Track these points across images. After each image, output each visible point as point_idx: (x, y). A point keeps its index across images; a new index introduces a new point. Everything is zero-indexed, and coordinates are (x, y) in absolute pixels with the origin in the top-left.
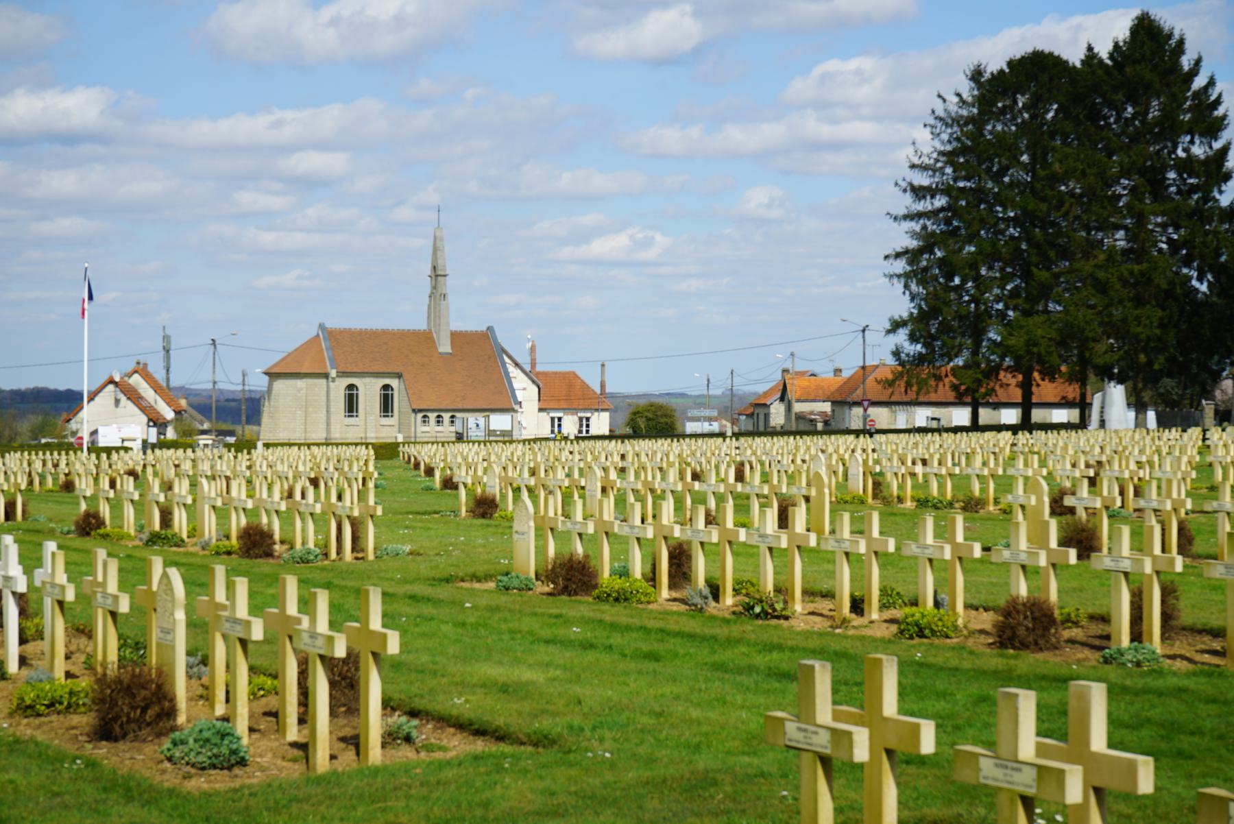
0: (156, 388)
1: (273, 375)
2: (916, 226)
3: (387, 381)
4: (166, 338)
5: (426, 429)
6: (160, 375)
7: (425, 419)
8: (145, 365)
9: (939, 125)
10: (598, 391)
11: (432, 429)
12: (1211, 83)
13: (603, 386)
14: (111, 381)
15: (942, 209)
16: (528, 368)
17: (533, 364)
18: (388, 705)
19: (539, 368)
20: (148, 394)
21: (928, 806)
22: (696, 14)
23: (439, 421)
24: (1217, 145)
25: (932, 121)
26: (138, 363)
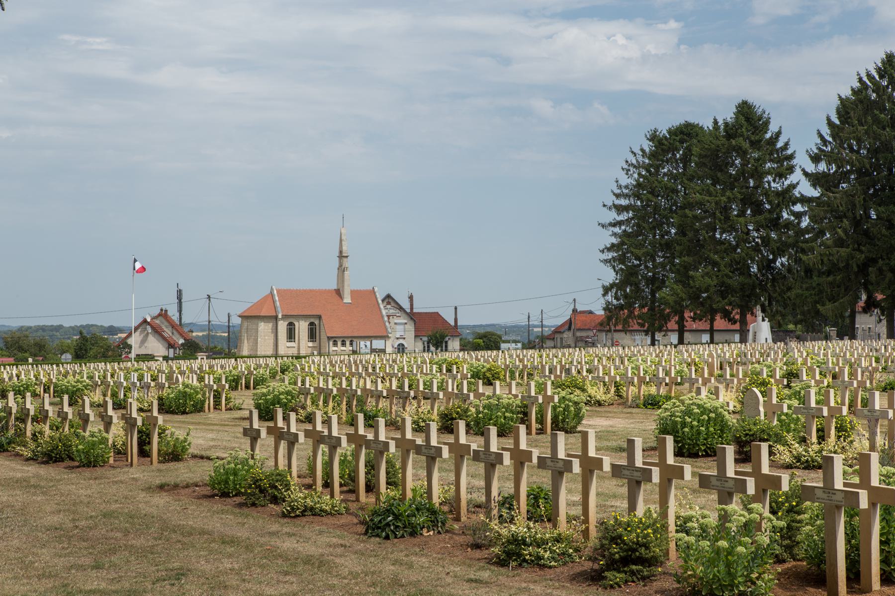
0: (173, 326)
1: (243, 317)
2: (617, 230)
3: (312, 320)
4: (180, 294)
5: (335, 348)
6: (175, 318)
7: (335, 344)
8: (166, 311)
9: (631, 168)
10: (453, 323)
11: (340, 348)
12: (787, 144)
13: (456, 320)
14: (145, 321)
15: (632, 219)
16: (408, 311)
17: (412, 308)
18: (598, 494)
19: (415, 311)
20: (168, 332)
21: (207, 561)
22: (676, 21)
23: (344, 344)
24: (787, 183)
25: (626, 167)
26: (162, 310)
